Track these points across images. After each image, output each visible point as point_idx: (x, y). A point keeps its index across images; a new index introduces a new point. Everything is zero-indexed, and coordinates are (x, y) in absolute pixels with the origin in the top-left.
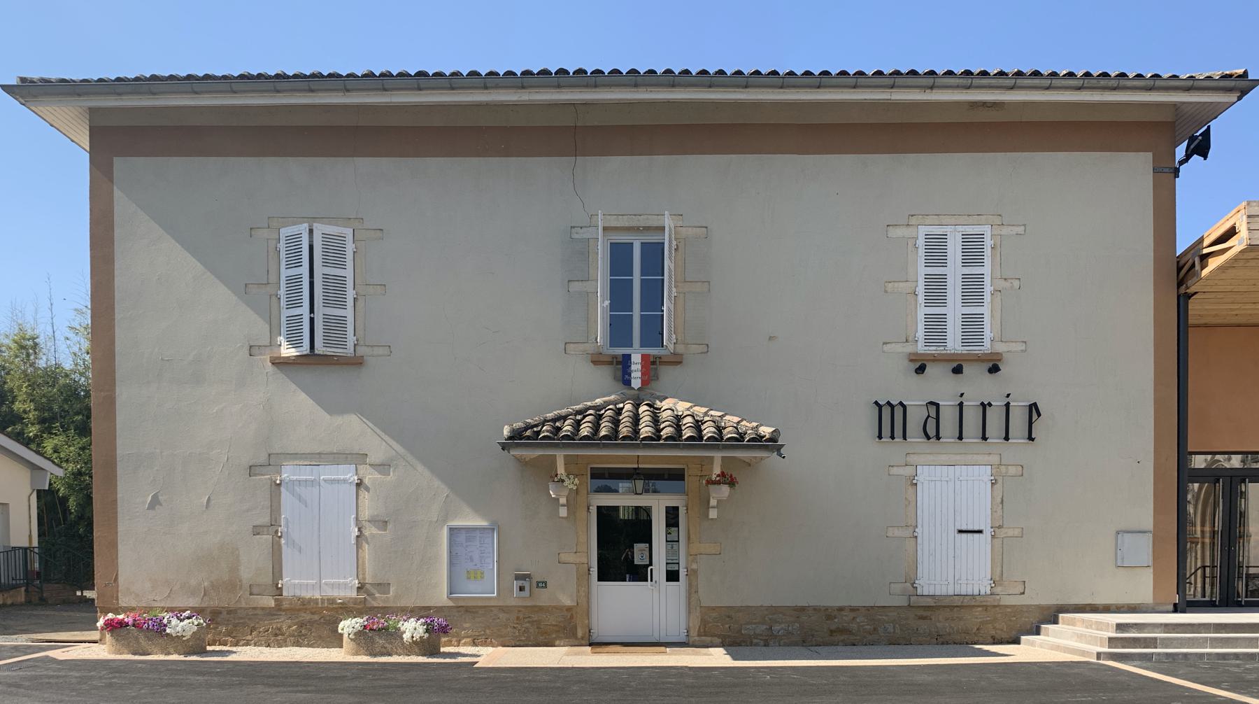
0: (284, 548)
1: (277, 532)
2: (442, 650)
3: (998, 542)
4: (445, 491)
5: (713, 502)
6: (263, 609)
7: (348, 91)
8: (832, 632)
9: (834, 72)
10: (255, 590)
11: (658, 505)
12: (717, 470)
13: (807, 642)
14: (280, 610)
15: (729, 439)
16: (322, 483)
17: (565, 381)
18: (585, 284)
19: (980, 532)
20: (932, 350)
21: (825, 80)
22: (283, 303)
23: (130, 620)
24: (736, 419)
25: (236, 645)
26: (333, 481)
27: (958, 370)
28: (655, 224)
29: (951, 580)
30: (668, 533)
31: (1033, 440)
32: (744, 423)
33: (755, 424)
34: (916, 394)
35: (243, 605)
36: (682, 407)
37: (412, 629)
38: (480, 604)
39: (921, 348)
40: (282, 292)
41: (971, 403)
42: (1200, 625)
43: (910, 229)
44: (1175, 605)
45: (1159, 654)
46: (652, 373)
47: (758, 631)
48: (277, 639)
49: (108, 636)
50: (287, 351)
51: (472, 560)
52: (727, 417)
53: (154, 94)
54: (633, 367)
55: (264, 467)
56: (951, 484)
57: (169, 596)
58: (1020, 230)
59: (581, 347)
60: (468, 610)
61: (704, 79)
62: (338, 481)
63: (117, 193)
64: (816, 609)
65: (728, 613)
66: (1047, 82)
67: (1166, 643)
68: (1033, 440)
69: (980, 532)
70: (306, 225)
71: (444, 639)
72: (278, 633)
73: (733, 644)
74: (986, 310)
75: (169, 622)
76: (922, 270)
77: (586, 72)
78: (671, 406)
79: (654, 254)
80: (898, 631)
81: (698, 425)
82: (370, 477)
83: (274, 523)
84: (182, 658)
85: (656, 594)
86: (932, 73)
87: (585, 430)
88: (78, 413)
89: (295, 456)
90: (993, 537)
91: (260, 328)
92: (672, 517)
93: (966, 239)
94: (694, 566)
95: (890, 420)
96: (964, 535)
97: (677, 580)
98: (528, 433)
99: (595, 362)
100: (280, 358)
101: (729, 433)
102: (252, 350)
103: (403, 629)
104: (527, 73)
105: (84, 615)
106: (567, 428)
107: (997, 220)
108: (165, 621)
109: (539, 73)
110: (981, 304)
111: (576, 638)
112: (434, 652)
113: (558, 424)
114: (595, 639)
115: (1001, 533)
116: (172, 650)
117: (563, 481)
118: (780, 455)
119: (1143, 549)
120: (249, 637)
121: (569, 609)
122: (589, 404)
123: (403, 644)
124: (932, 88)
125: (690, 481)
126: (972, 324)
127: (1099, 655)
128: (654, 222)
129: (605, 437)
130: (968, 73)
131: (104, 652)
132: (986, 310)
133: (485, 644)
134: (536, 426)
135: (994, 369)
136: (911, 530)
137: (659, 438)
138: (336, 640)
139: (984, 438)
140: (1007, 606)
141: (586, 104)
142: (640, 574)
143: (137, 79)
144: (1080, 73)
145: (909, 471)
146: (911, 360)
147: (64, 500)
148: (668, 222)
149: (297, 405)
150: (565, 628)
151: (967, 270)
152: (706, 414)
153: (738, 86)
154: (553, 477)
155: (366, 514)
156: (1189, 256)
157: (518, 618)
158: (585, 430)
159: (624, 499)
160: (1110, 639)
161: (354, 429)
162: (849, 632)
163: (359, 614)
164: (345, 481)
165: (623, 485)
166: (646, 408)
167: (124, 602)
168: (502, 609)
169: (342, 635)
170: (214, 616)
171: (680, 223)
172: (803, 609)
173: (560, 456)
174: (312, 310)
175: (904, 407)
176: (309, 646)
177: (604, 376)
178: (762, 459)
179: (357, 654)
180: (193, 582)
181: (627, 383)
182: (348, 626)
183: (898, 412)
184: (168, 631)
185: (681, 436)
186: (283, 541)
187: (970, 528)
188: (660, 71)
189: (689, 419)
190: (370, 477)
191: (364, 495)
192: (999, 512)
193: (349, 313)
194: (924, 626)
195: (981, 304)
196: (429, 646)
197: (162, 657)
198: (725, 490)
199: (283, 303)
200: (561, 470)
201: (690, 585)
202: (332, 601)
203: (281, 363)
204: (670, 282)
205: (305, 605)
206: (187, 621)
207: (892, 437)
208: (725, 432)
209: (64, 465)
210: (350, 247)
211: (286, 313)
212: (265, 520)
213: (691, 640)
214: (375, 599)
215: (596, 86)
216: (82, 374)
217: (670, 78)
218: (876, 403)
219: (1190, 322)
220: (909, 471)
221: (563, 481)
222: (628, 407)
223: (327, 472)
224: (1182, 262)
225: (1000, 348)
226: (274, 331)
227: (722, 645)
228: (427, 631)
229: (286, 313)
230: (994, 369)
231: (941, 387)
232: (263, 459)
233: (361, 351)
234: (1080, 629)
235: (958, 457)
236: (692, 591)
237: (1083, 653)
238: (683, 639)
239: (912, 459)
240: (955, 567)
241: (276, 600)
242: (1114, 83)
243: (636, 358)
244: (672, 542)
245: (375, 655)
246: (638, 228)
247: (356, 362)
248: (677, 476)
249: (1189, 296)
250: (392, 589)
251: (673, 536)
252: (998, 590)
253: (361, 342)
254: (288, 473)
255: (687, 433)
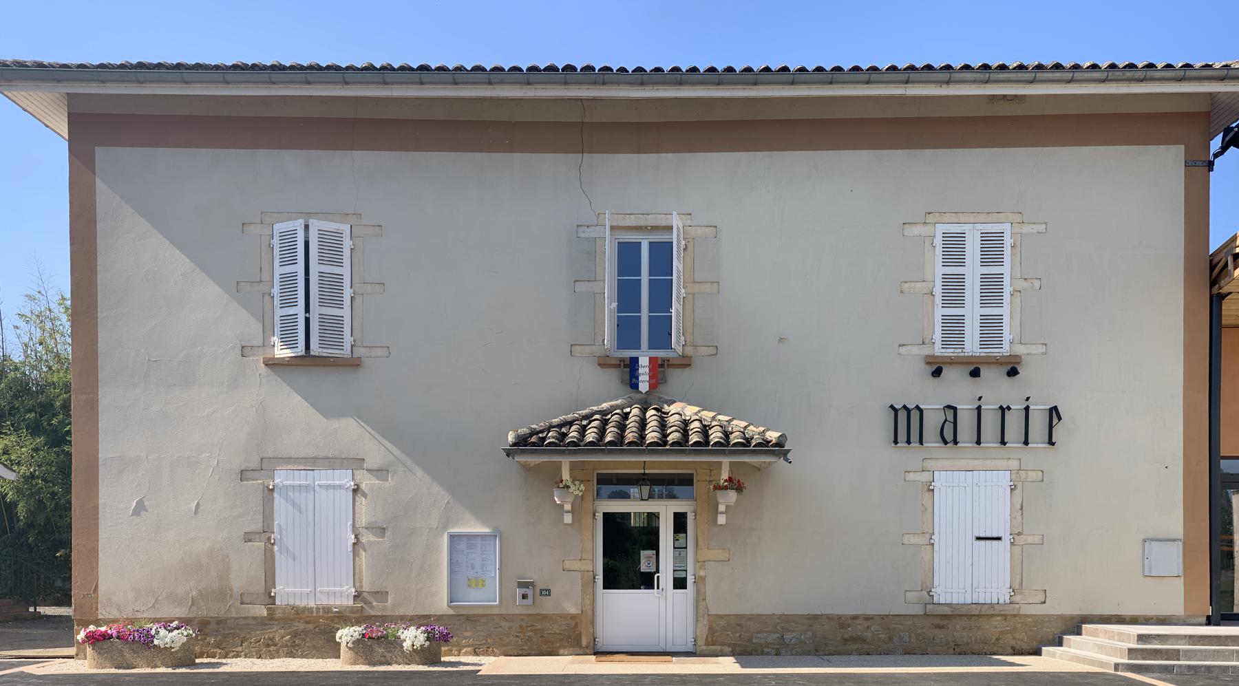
0: (277, 555)
1: (269, 539)
2: (443, 659)
3: (1017, 549)
4: (445, 497)
5: (722, 508)
6: (255, 618)
7: (347, 83)
8: (846, 640)
9: (846, 67)
10: (246, 599)
11: (666, 511)
12: (725, 475)
13: (819, 650)
14: (272, 619)
15: (735, 444)
16: (317, 488)
17: (571, 386)
18: (591, 284)
19: (999, 539)
20: (949, 352)
21: (837, 76)
22: (277, 302)
23: (114, 632)
24: (743, 424)
25: (226, 657)
26: (328, 487)
27: (975, 373)
28: (664, 224)
29: (969, 589)
30: (675, 540)
31: (1053, 444)
32: (751, 427)
33: (761, 429)
34: (932, 398)
35: (234, 615)
36: (690, 411)
37: (412, 637)
38: (481, 612)
39: (938, 350)
40: (276, 290)
41: (989, 407)
42: (1227, 637)
43: (929, 227)
44: (1208, 617)
45: (1180, 666)
46: (660, 377)
47: (769, 640)
48: (270, 649)
49: (89, 650)
50: (281, 352)
51: (473, 568)
52: (735, 422)
53: (141, 82)
54: (641, 371)
55: (256, 471)
56: (969, 490)
57: (154, 606)
58: (1042, 228)
59: (588, 349)
60: (469, 619)
61: (712, 76)
62: (334, 487)
63: (100, 185)
64: (829, 618)
65: (740, 622)
66: (1068, 76)
67: (1189, 655)
68: (1053, 444)
69: (999, 539)
70: (301, 222)
71: (444, 649)
72: (270, 643)
73: (743, 652)
74: (1005, 311)
75: (157, 633)
76: (940, 270)
77: (593, 69)
78: (679, 410)
79: (662, 253)
80: (913, 640)
81: (705, 430)
82: (367, 482)
83: (267, 529)
84: (170, 670)
85: (662, 603)
86: (948, 67)
87: (590, 436)
88: (30, 411)
89: (289, 460)
90: (1012, 544)
91: (253, 328)
92: (680, 523)
93: (985, 237)
94: (702, 573)
95: (906, 424)
96: (982, 542)
97: (684, 587)
98: (534, 439)
99: (602, 365)
100: (274, 359)
101: (735, 438)
102: (244, 351)
103: (402, 637)
104: (533, 69)
105: (42, 631)
106: (573, 434)
107: (1018, 218)
108: (153, 632)
109: (545, 69)
110: (1000, 305)
111: (581, 647)
112: (435, 661)
113: (564, 430)
114: (600, 648)
115: (1020, 540)
116: (159, 663)
117: (568, 487)
118: (787, 460)
119: (1171, 559)
120: (240, 649)
121: (573, 617)
122: (595, 408)
123: (403, 652)
124: (948, 82)
125: (699, 487)
126: (991, 326)
127: (1117, 667)
128: (662, 221)
129: (610, 443)
130: (986, 67)
131: (83, 666)
132: (1005, 311)
133: (486, 654)
134: (541, 432)
135: (1013, 372)
136: (927, 536)
137: (665, 443)
138: (333, 649)
139: (1003, 442)
140: (1027, 616)
141: (594, 100)
142: (647, 581)
143: (122, 66)
144: (1104, 65)
145: (925, 477)
146: (927, 363)
147: (14, 505)
148: (676, 222)
149: (292, 407)
150: (569, 637)
151: (987, 270)
152: (713, 418)
153: (747, 84)
154: (558, 482)
155: (363, 520)
156: (1222, 255)
157: (521, 627)
158: (590, 436)
159: (634, 506)
160: (1130, 650)
161: (351, 433)
162: (864, 641)
163: (358, 622)
164: (340, 487)
165: (634, 491)
166: (653, 412)
167: (102, 614)
168: (503, 617)
169: (339, 644)
170: (203, 626)
171: (688, 223)
172: (816, 617)
173: (566, 462)
174: (307, 310)
175: (921, 411)
176: (303, 656)
177: (611, 379)
178: (770, 464)
179: (355, 663)
180: (180, 591)
181: (635, 386)
182: (346, 635)
183: (915, 416)
184: (156, 642)
185: (687, 441)
186: (276, 548)
187: (988, 535)
188: (667, 68)
189: (696, 424)
190: (367, 482)
191: (361, 500)
192: (1019, 518)
193: (346, 312)
194: (940, 635)
195: (1000, 305)
196: (429, 655)
197: (149, 670)
198: (732, 496)
199: (277, 302)
200: (566, 476)
201: (698, 592)
202: (327, 609)
203: (273, 365)
204: (678, 284)
205: (299, 613)
206: (176, 632)
207: (909, 442)
208: (732, 437)
209: (15, 468)
210: (347, 244)
211: (279, 312)
212: (257, 526)
213: (699, 649)
214: (372, 607)
215: (604, 83)
216: (33, 367)
217: (677, 76)
218: (892, 407)
219: (1224, 322)
220: (925, 477)
221: (568, 487)
222: (635, 411)
223: (323, 477)
224: (1215, 262)
225: (1019, 350)
226: (267, 331)
227: (732, 654)
228: (428, 639)
229: (279, 312)
230: (1013, 372)
231: (958, 390)
232: (255, 463)
233: (359, 352)
234: (1102, 640)
235: (976, 462)
236: (699, 598)
237: (1102, 664)
238: (690, 648)
239: (929, 464)
240: (969, 574)
241: (268, 609)
242: (1140, 74)
243: (644, 361)
244: (679, 548)
245: (374, 665)
246: (646, 227)
247: (353, 364)
248: (687, 480)
249: (1222, 297)
250: (390, 598)
251: (681, 543)
252: (1018, 598)
253: (359, 343)
254: (281, 478)
255: (694, 438)
